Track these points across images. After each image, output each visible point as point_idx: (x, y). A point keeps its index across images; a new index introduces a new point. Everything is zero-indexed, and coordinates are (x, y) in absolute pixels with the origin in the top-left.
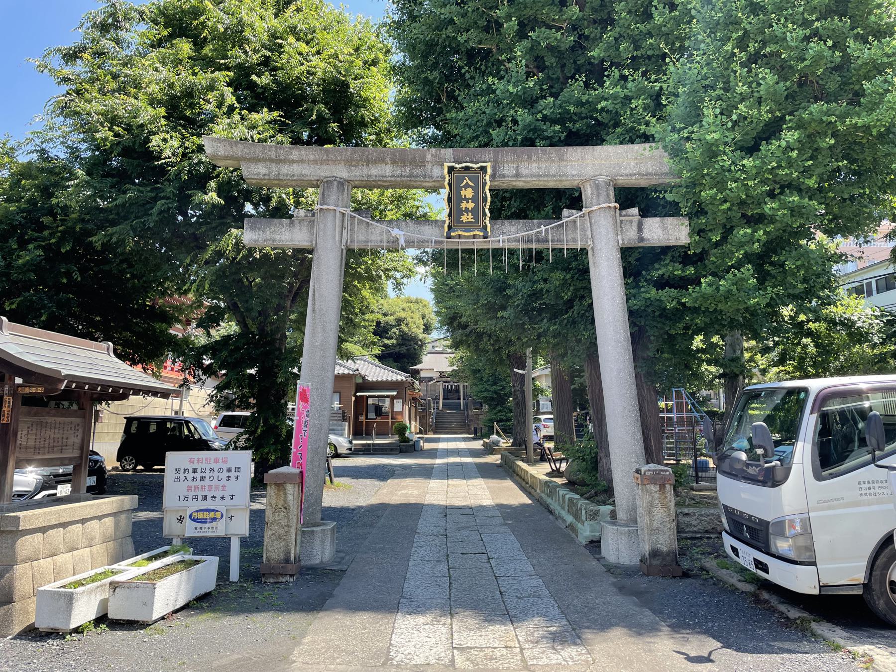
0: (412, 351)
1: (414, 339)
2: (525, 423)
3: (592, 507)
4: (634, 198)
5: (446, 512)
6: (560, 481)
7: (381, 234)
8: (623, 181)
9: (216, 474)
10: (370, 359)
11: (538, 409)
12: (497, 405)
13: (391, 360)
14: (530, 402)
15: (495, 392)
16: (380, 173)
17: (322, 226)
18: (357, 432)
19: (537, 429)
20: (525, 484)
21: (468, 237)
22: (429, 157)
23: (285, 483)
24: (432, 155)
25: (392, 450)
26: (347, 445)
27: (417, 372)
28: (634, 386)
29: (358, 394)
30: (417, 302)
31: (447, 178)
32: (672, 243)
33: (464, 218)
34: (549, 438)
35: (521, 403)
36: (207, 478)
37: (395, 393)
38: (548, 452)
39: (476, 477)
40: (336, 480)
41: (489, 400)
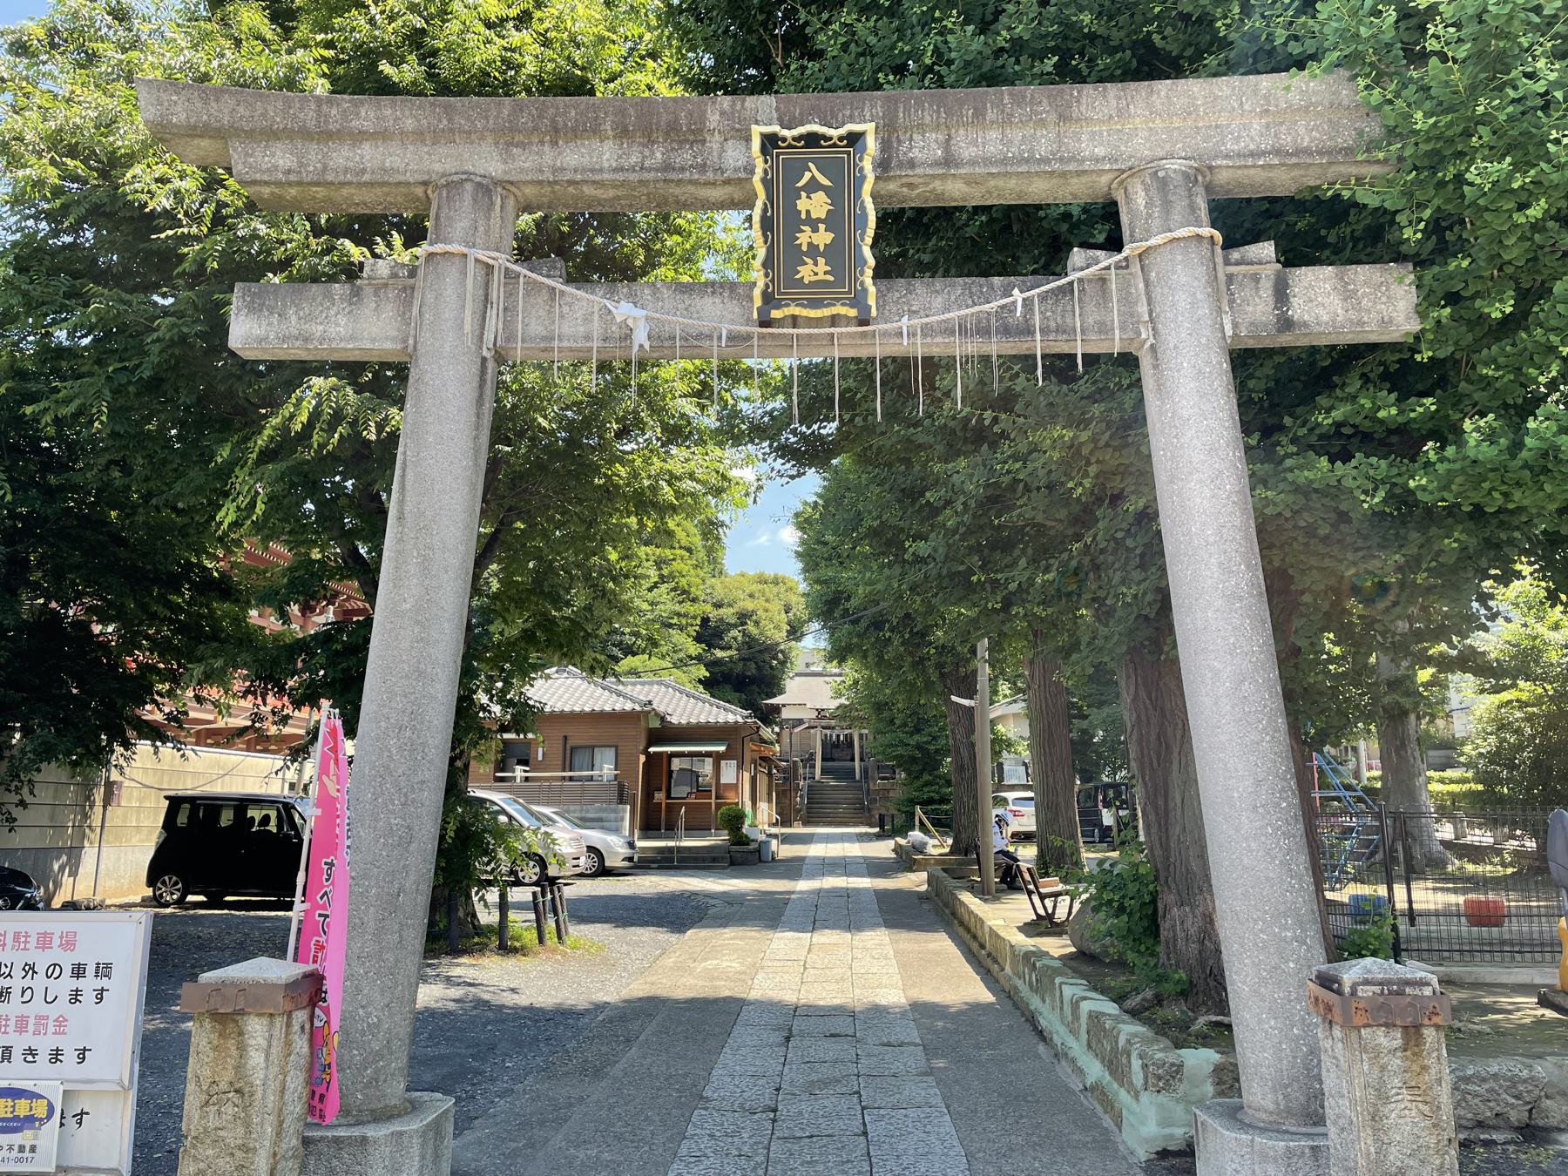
0: (767, 672)
1: (771, 649)
2: (975, 808)
3: (1161, 1052)
5: (791, 1024)
6: (1057, 946)
7: (587, 319)
9: (39, 982)
10: (689, 688)
11: (1001, 779)
13: (728, 687)
14: (986, 767)
15: (919, 747)
16: (586, 160)
17: (430, 297)
18: (649, 826)
19: (1001, 821)
20: (979, 950)
21: (817, 322)
22: (713, 119)
23: (242, 1012)
24: (723, 113)
25: (714, 860)
26: (625, 851)
27: (777, 709)
28: (1281, 721)
29: (652, 750)
30: (776, 582)
33: (806, 272)
34: (1023, 838)
35: (968, 768)
36: (16, 992)
37: (722, 749)
38: (1027, 877)
39: (873, 926)
40: (575, 931)
41: (906, 763)
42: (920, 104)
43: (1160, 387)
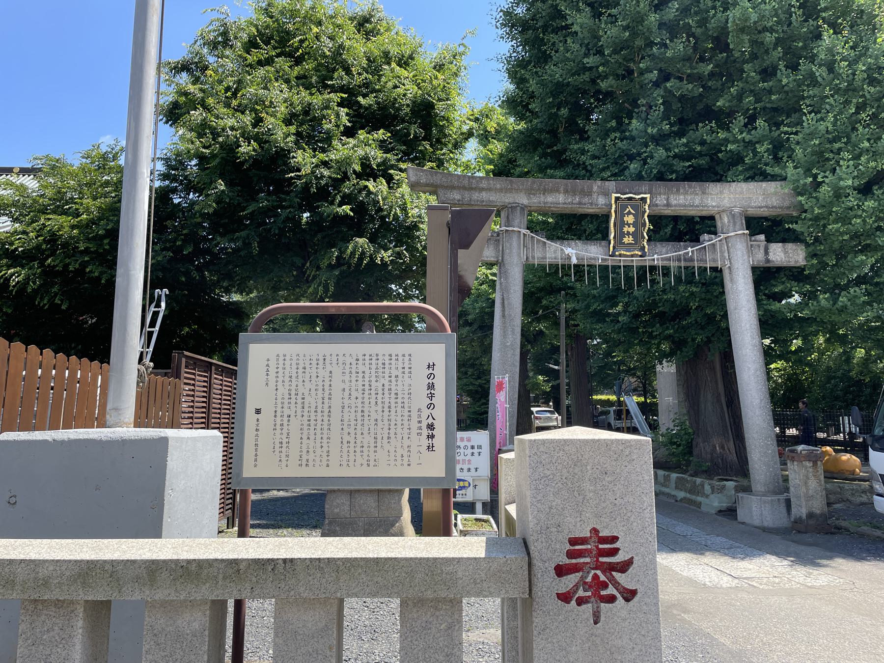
4: (766, 227)
8: (752, 212)
12: (480, 399)
15: (480, 386)
22: (595, 188)
31: (614, 206)
32: (792, 264)
33: (626, 240)
42: (660, 187)
43: (732, 280)
